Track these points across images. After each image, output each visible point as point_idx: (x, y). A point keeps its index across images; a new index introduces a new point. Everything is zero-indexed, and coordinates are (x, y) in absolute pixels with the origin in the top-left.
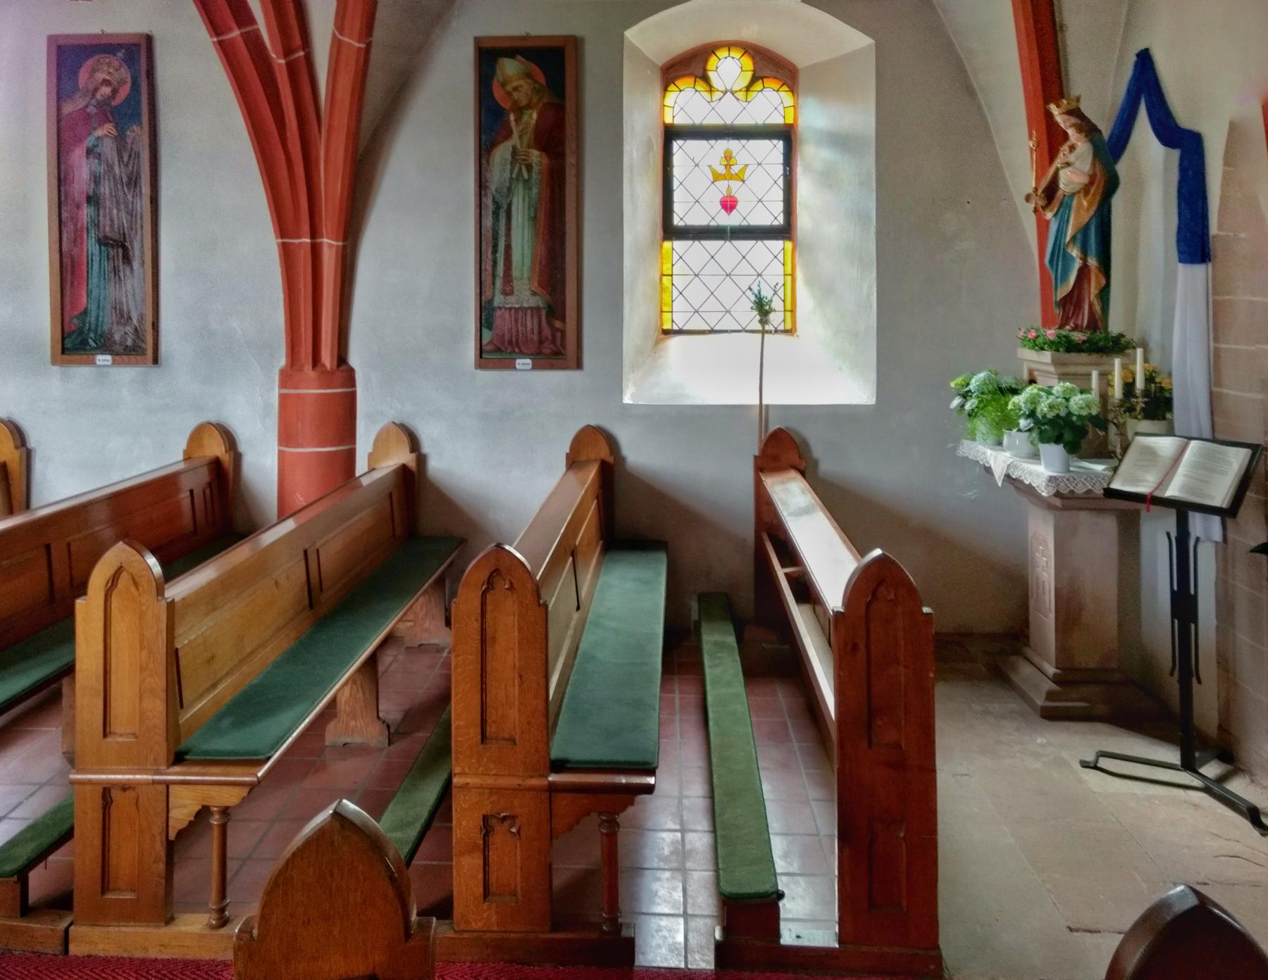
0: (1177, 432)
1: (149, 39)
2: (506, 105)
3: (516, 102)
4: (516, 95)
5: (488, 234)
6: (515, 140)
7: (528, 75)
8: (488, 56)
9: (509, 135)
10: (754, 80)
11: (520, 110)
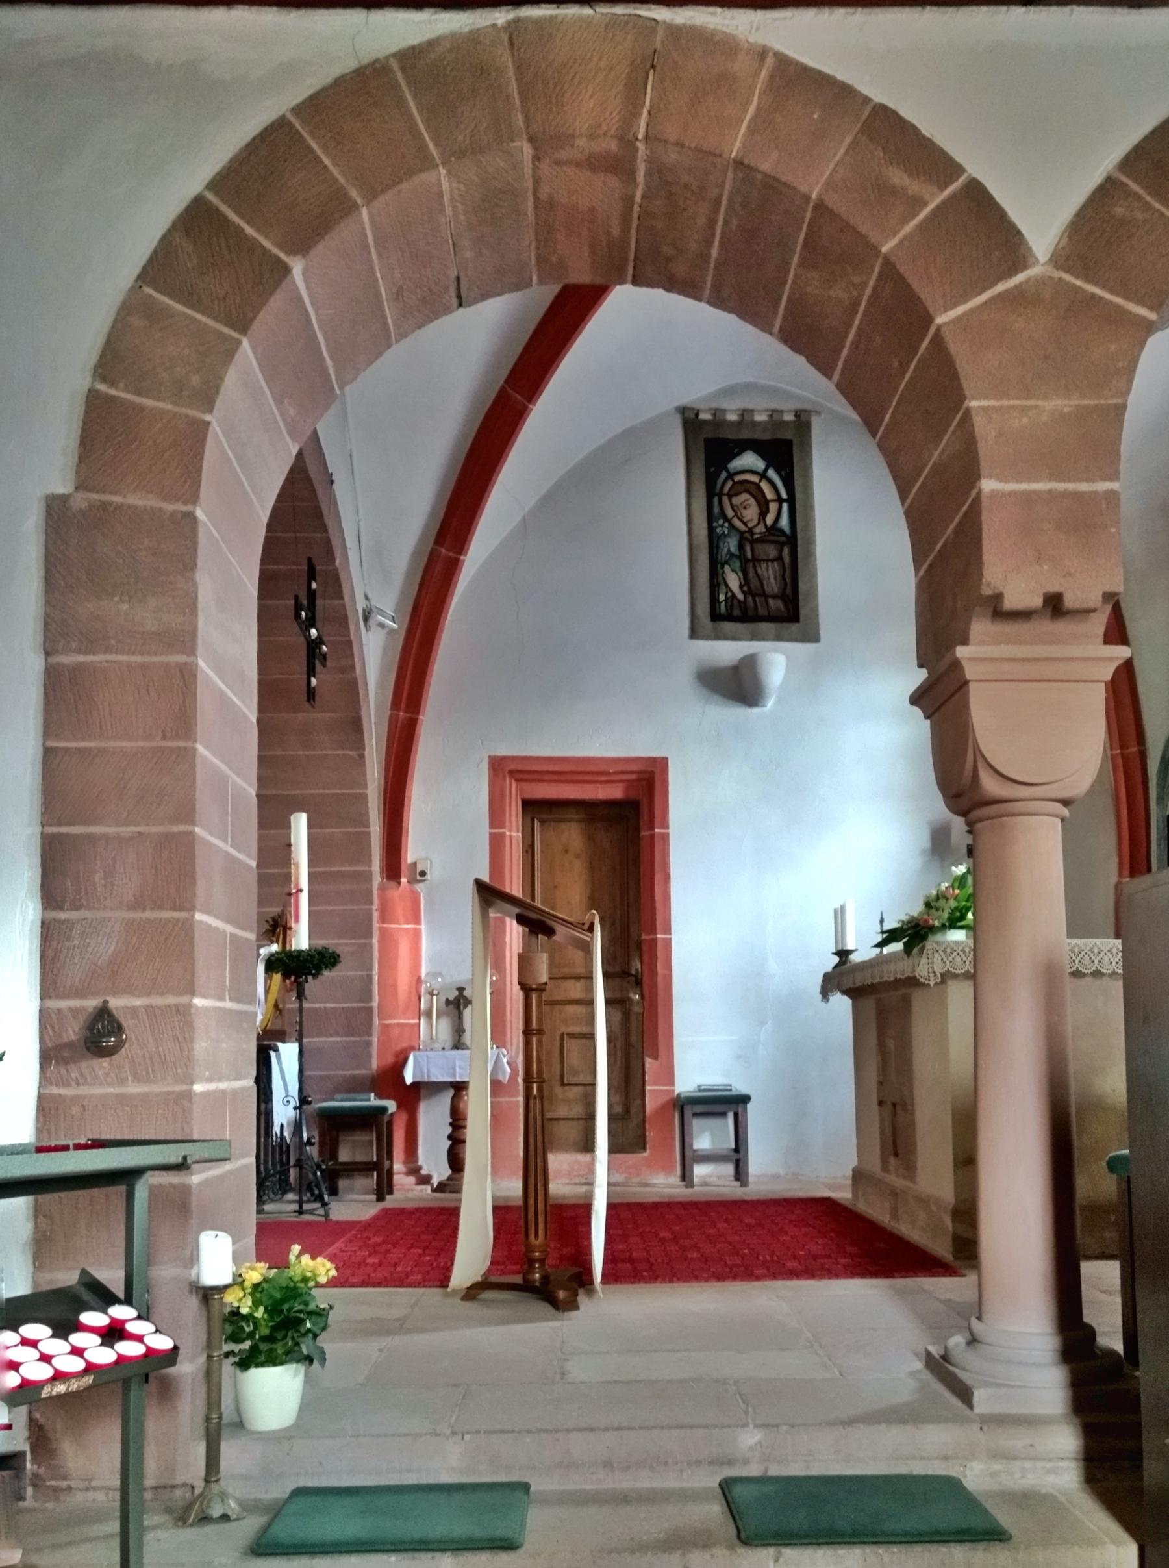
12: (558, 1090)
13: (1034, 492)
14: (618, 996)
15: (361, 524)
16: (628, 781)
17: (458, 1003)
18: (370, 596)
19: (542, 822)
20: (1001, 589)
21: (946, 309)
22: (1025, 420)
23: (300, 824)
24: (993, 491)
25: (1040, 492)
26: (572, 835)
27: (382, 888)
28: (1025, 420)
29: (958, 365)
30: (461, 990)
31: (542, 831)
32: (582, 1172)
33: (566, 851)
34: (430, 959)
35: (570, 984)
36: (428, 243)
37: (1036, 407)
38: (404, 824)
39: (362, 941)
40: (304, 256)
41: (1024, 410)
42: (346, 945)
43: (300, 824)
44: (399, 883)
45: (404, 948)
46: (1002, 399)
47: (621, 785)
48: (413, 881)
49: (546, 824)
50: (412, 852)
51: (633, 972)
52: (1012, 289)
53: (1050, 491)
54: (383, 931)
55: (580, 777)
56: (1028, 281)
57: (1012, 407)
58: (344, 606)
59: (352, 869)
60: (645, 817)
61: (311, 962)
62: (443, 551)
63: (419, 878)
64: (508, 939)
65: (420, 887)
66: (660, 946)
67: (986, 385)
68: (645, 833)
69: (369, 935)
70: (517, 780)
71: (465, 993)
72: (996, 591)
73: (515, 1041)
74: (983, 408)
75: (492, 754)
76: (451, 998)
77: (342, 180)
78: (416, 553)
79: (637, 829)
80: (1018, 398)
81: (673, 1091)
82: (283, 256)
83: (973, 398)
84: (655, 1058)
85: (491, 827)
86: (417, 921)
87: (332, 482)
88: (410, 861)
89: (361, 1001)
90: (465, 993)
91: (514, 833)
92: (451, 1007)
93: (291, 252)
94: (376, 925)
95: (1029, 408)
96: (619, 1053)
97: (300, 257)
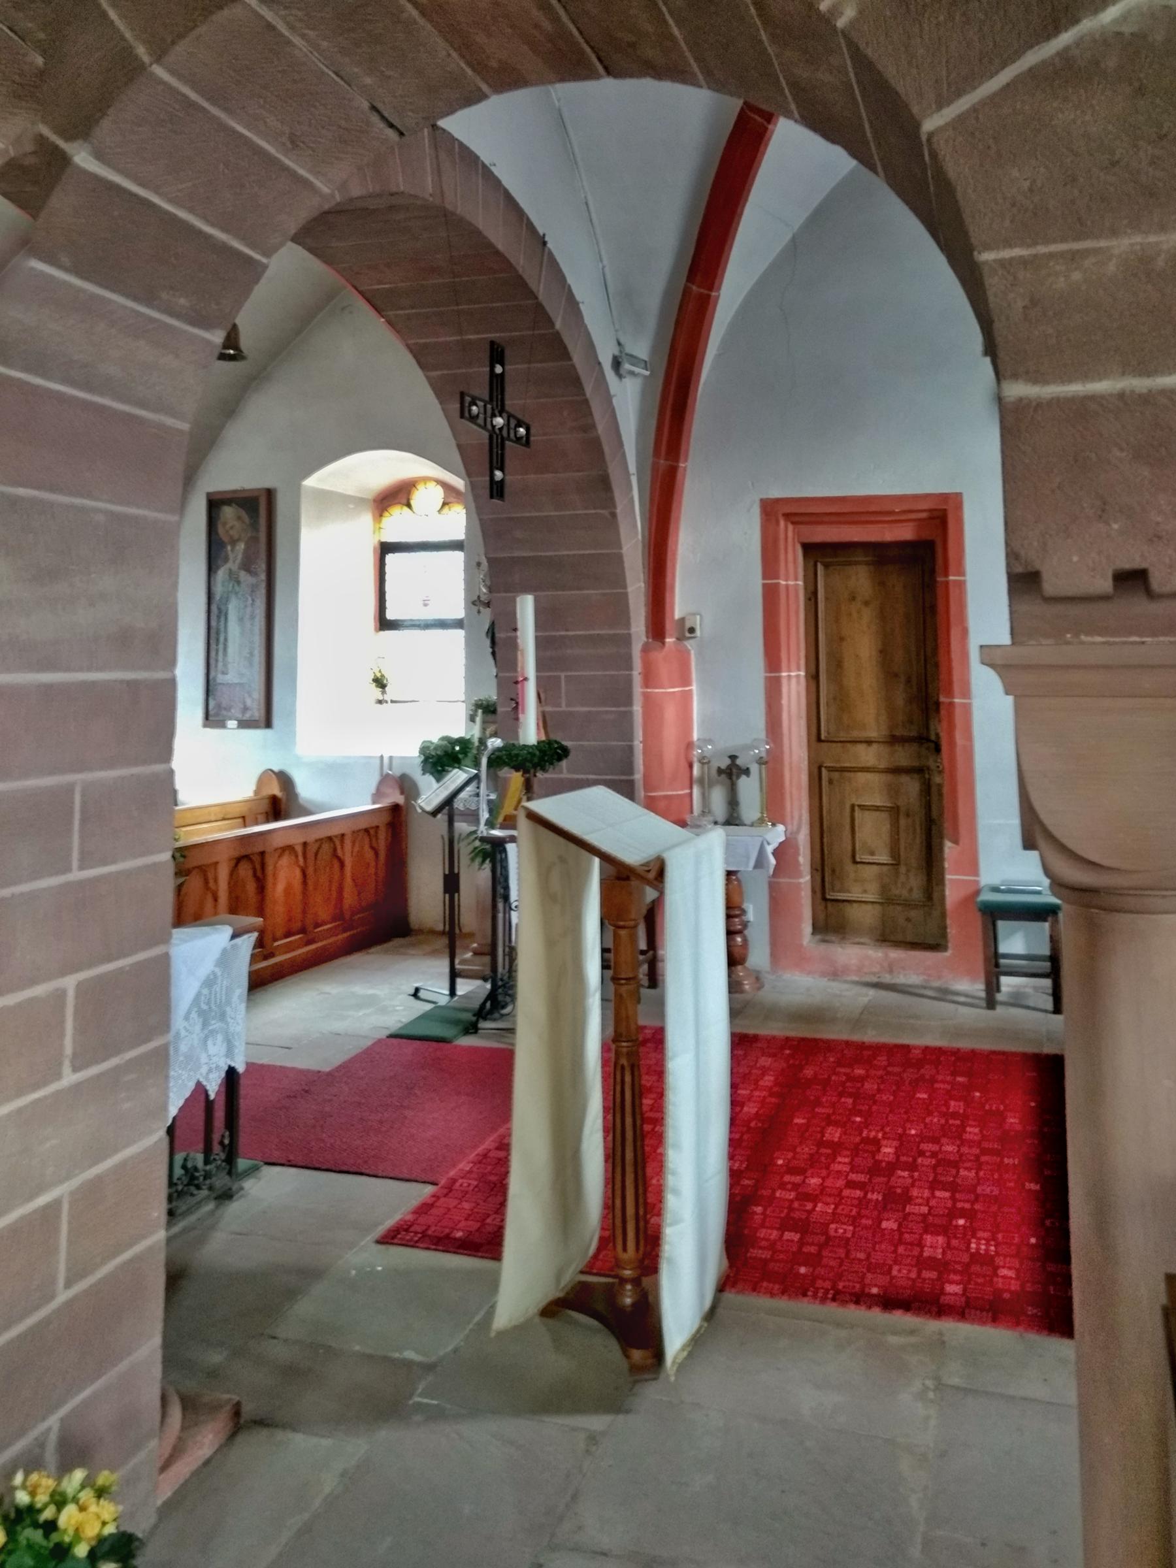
0: (730, 1296)
1: (270, 494)
2: (225, 539)
3: (231, 537)
4: (231, 532)
5: (222, 619)
6: (229, 565)
7: (239, 518)
8: (215, 504)
9: (226, 560)
10: (444, 504)
11: (234, 542)
12: (850, 868)
13: (1092, 398)
14: (916, 764)
15: (607, 270)
16: (920, 520)
17: (732, 772)
18: (622, 341)
19: (826, 566)
20: (1038, 566)
21: (941, 103)
22: (1077, 276)
23: (526, 607)
24: (1021, 399)
25: (1102, 397)
26: (860, 579)
27: (646, 649)
28: (1077, 276)
29: (959, 196)
30: (733, 758)
31: (827, 576)
32: (874, 970)
33: (854, 598)
34: (702, 723)
35: (861, 748)
36: (295, 81)
37: (1096, 251)
38: (668, 580)
39: (622, 709)
40: (85, 140)
41: (1074, 257)
42: (607, 712)
43: (526, 607)
44: (663, 643)
45: (670, 713)
46: (1035, 244)
47: (911, 524)
48: (681, 638)
49: (831, 568)
50: (679, 606)
51: (933, 737)
52: (1052, 58)
53: (1121, 395)
54: (646, 696)
55: (863, 518)
56: (1078, 43)
57: (1051, 256)
58: (573, 366)
59: (612, 632)
60: (940, 562)
61: (531, 761)
62: (694, 288)
63: (688, 635)
64: (784, 702)
65: (690, 645)
66: (958, 712)
67: (1007, 223)
68: (940, 579)
69: (629, 701)
70: (793, 523)
71: (738, 762)
72: (1030, 569)
73: (796, 814)
74: (1002, 263)
75: (764, 496)
76: (723, 766)
77: (128, 35)
78: (667, 294)
79: (933, 572)
80: (1064, 240)
81: (977, 882)
82: (61, 143)
83: (987, 247)
84: (956, 842)
85: (764, 578)
86: (685, 680)
87: (545, 243)
88: (677, 616)
89: (623, 774)
90: (738, 762)
91: (793, 581)
92: (723, 776)
93: (69, 138)
94: (638, 689)
95: (1085, 253)
96: (918, 831)
97: (80, 142)
